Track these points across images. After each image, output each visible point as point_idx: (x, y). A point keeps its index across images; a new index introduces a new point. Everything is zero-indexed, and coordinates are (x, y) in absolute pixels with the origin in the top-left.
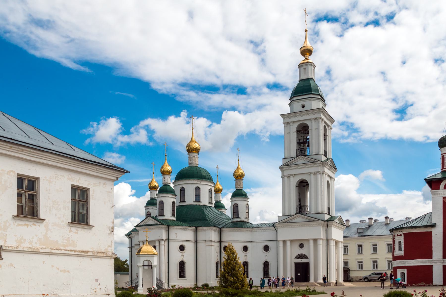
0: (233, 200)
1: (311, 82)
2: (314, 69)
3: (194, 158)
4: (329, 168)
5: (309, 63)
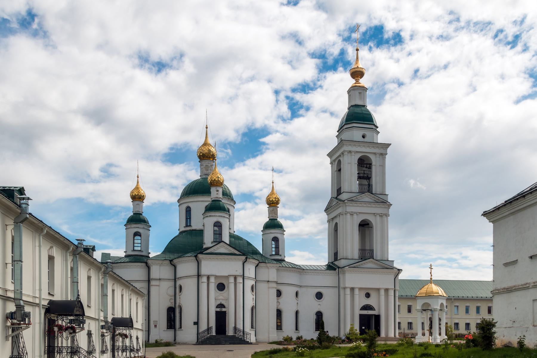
4: (339, 206)
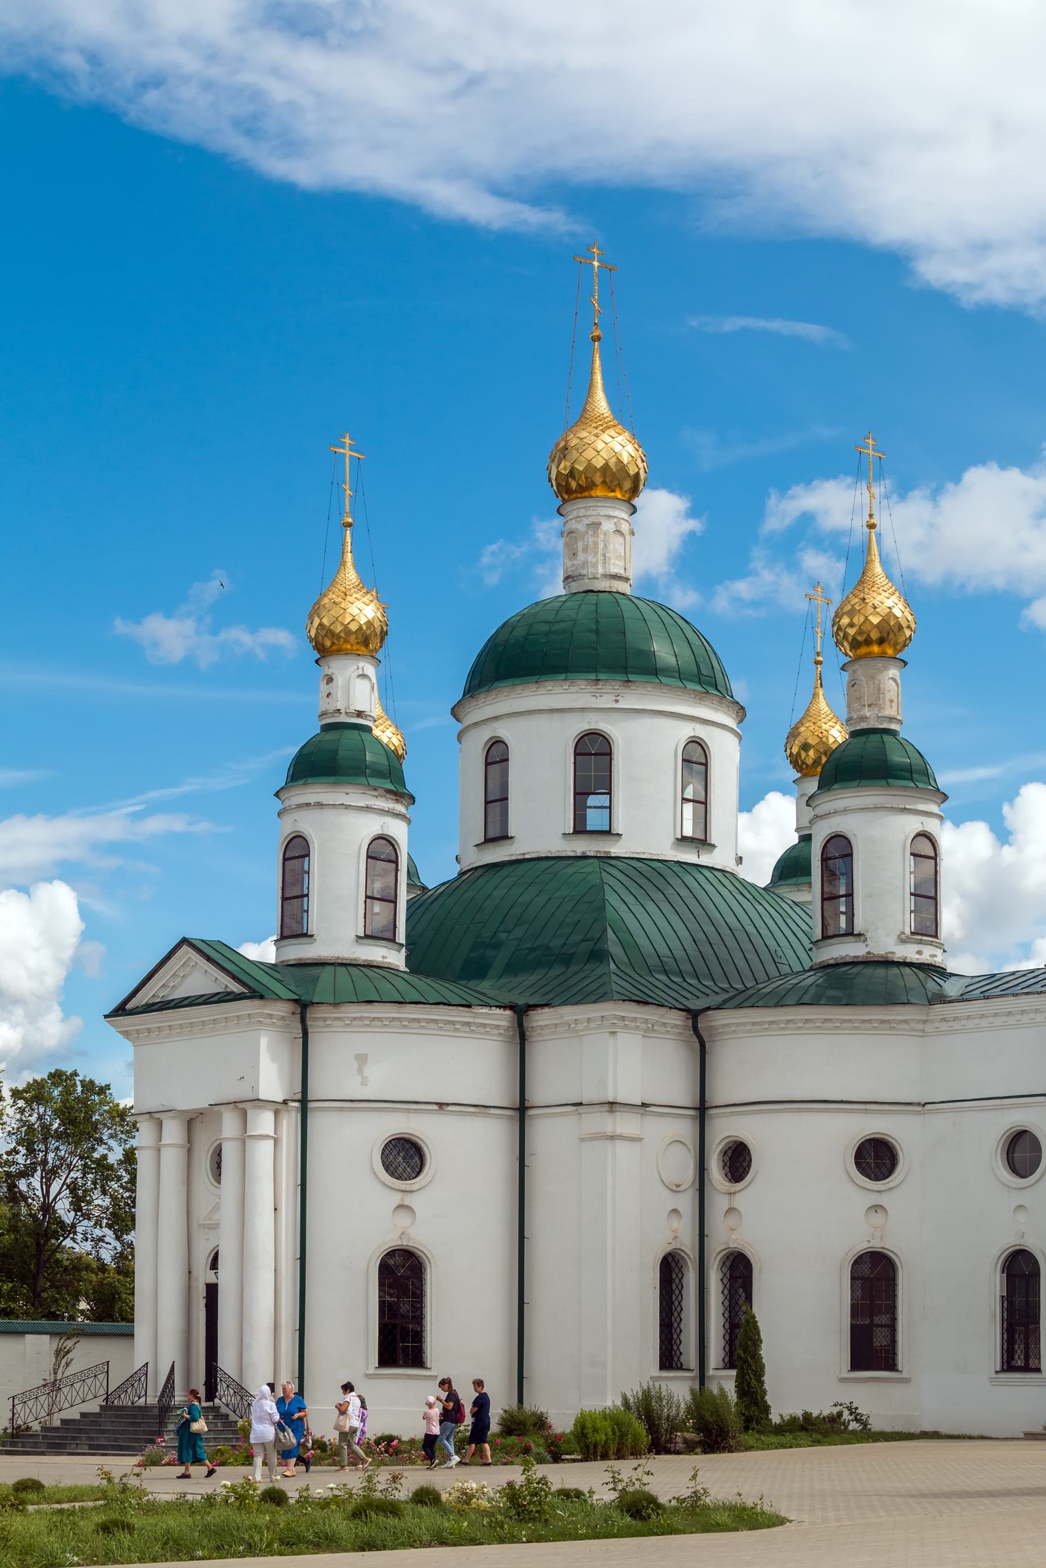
3: (595, 533)
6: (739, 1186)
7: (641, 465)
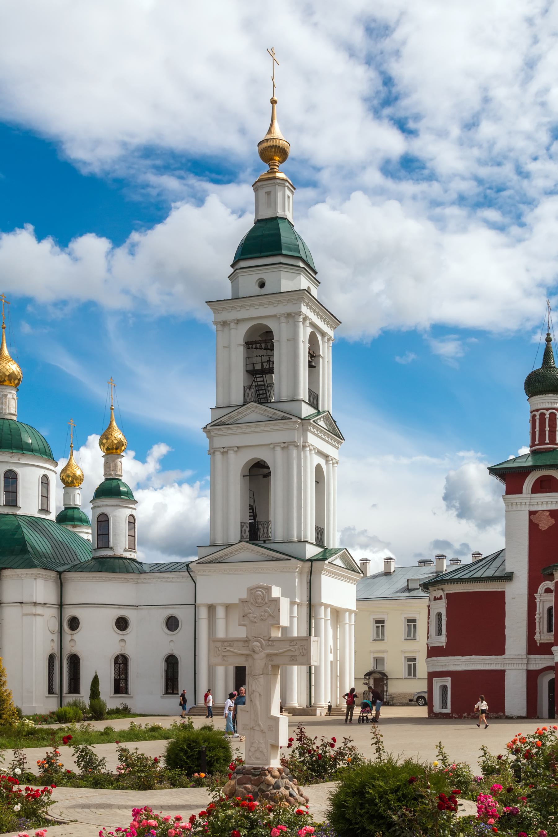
0: (96, 504)
1: (282, 226)
2: (290, 195)
5: (278, 181)
6: (75, 632)
7: (21, 375)
